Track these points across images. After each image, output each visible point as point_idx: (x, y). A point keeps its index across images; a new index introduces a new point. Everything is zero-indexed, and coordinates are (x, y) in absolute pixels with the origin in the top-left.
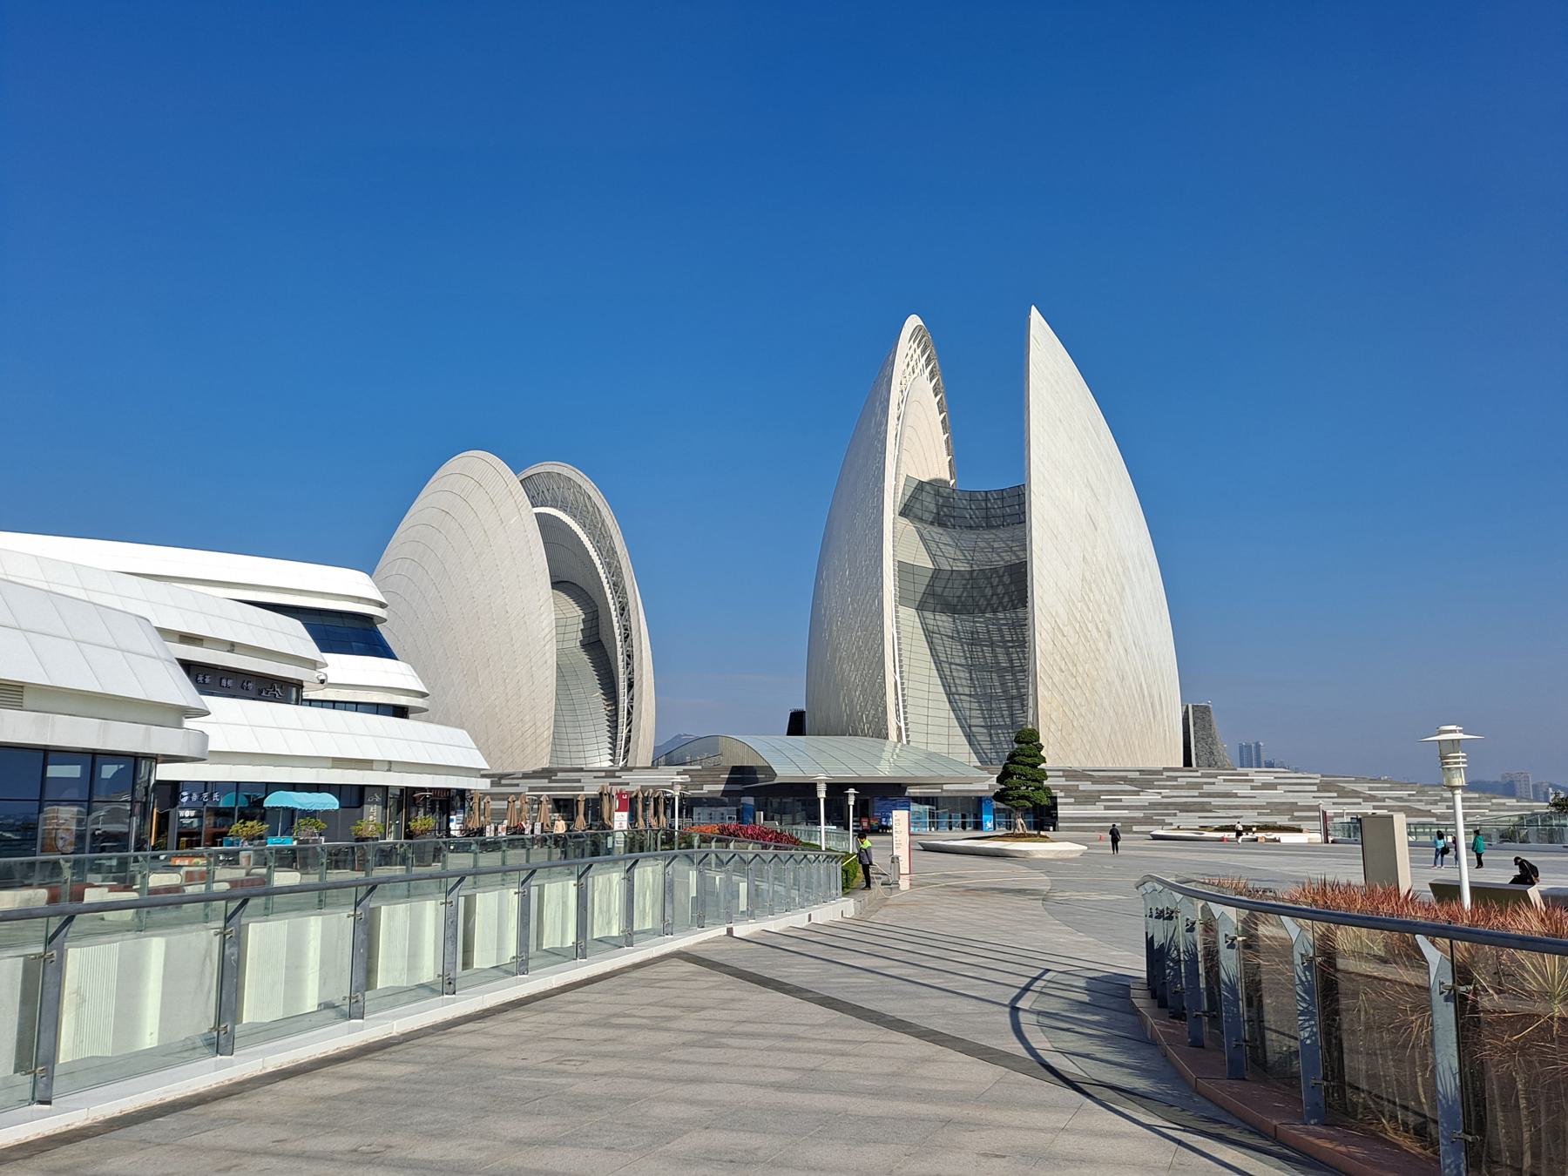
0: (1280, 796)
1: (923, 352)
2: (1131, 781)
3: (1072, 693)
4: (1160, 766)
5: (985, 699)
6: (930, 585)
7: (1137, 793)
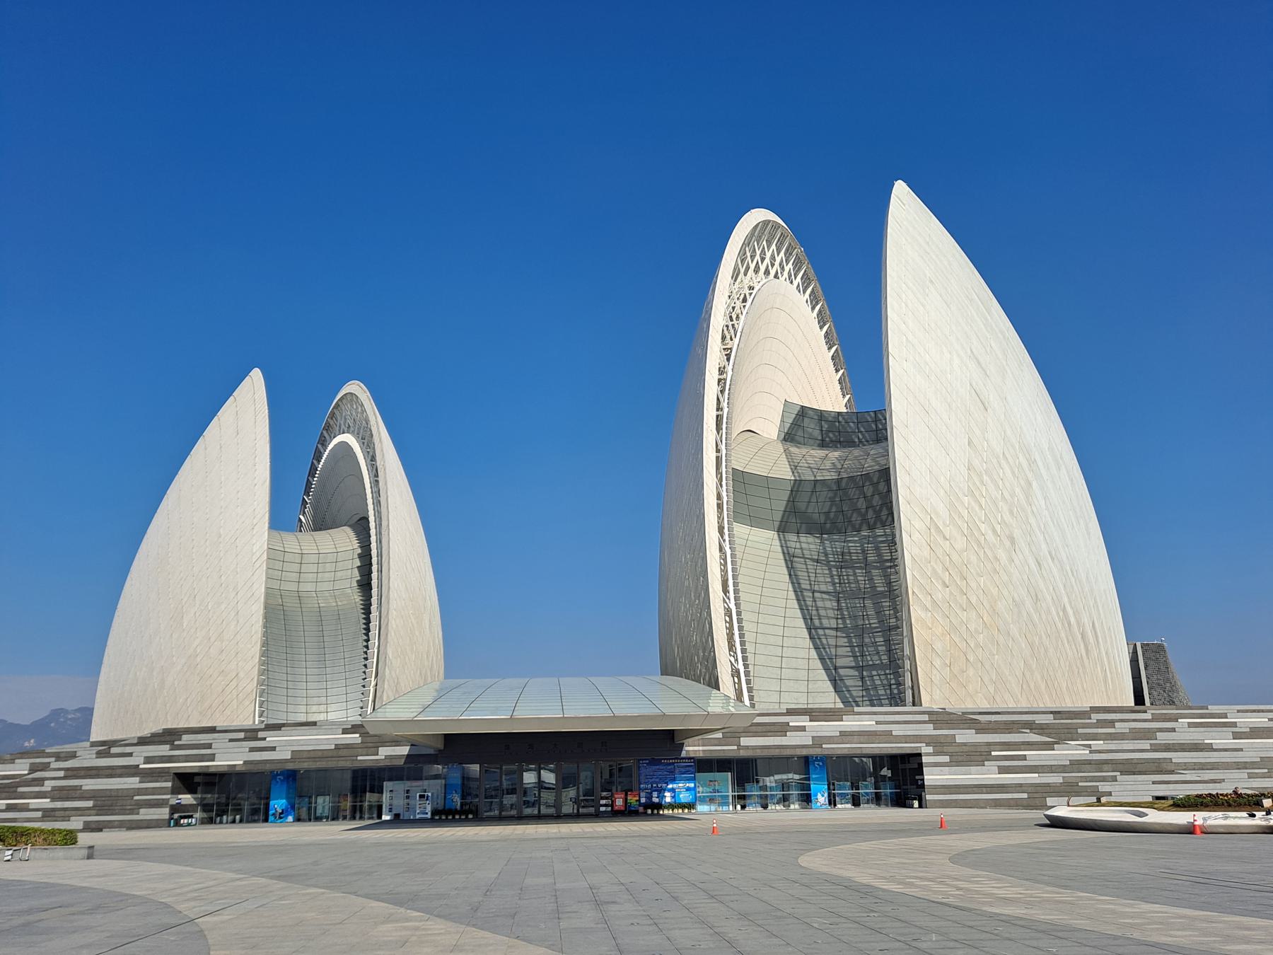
1: (788, 254)
3: (963, 616)
4: (1085, 704)
5: (857, 633)
6: (792, 501)
7: (1049, 746)
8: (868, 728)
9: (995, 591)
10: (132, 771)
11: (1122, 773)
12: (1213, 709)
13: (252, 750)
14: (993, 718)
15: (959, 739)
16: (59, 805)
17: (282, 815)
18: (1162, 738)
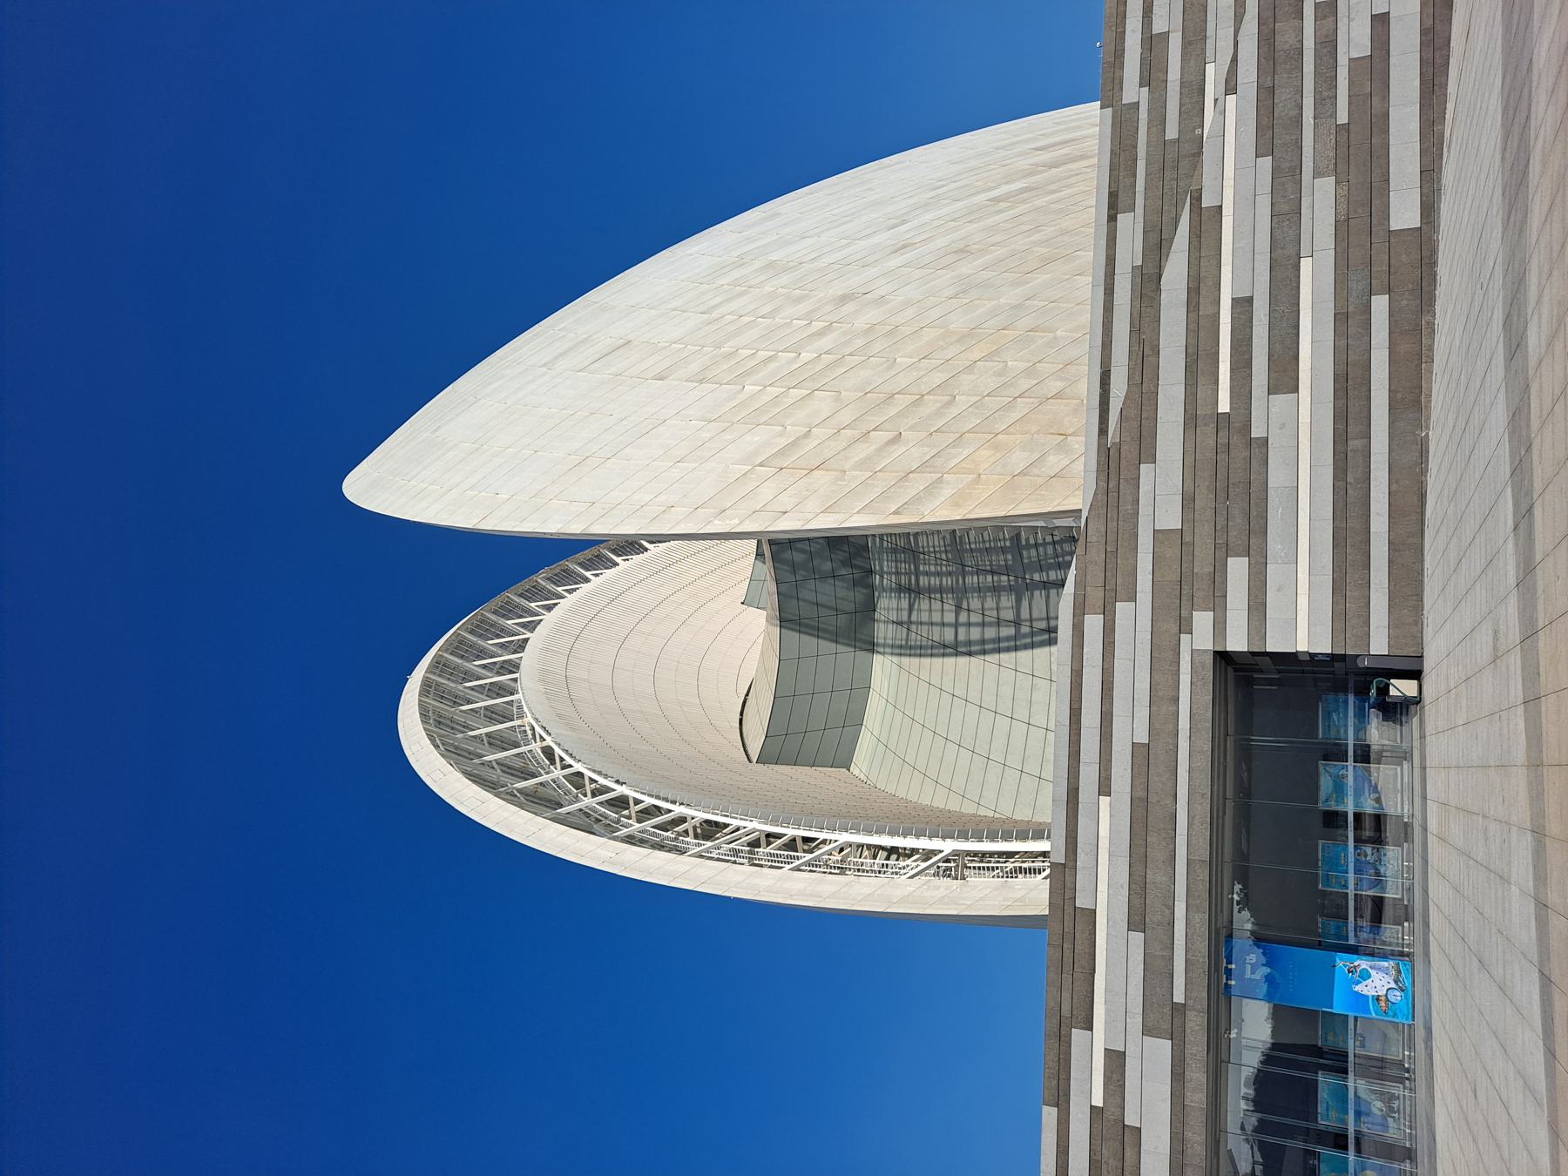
7: (1207, 223)
9: (929, 334)
15: (1171, 519)
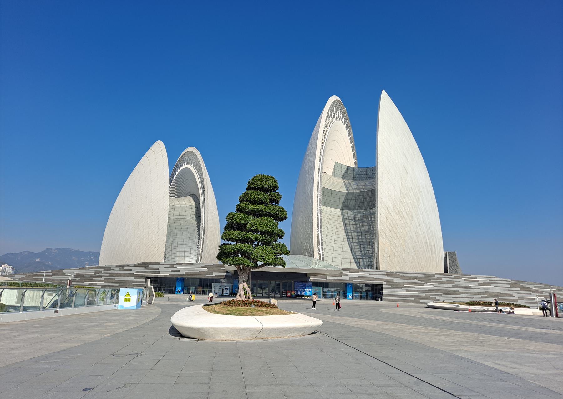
0: (492, 289)
2: (420, 279)
7: (422, 284)
8: (365, 276)
10: (132, 275)
11: (444, 294)
12: (472, 276)
13: (172, 271)
14: (405, 275)
16: (107, 284)
17: (180, 292)
18: (456, 284)
